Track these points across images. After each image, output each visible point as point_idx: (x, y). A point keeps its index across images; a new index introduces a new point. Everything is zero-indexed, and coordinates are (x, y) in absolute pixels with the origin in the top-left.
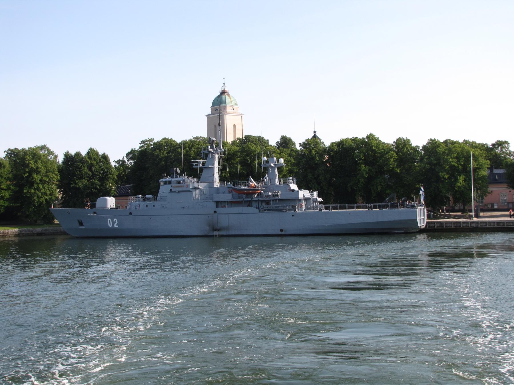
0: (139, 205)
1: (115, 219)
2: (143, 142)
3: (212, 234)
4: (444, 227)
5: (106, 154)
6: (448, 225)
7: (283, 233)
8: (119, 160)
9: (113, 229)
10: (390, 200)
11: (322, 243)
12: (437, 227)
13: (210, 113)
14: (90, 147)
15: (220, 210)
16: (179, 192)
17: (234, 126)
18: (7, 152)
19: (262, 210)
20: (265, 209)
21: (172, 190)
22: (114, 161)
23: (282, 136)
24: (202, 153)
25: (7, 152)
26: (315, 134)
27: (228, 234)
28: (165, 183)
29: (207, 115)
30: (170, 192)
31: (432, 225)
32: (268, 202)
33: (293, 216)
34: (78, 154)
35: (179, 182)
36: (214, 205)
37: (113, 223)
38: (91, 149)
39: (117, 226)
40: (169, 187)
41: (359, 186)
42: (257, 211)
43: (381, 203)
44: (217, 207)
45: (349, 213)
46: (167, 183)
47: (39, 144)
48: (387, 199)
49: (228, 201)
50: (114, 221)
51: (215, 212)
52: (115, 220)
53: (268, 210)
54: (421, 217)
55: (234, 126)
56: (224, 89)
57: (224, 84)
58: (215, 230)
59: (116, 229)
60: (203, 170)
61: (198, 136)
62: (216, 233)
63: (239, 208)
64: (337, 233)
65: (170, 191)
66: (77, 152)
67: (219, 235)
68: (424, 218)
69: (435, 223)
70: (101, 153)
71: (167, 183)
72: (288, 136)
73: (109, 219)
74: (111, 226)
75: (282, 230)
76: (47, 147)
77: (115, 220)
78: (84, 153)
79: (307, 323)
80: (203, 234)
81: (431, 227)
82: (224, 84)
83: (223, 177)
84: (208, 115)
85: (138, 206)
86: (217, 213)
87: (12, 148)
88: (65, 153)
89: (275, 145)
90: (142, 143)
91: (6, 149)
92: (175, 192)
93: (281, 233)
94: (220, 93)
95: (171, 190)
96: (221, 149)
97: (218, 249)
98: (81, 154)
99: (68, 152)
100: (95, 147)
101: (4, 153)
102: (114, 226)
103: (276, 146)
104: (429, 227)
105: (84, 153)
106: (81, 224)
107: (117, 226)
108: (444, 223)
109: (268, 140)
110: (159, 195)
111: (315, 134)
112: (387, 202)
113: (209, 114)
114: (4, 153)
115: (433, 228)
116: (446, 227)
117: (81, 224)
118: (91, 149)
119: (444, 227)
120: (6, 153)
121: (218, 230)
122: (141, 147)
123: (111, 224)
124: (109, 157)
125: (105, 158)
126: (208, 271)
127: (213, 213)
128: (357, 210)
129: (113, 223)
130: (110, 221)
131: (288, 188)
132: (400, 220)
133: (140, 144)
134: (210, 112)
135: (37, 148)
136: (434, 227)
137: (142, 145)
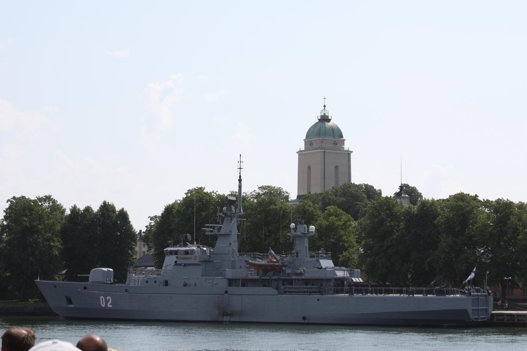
0: (138, 280)
1: (108, 297)
3: (222, 320)
4: (516, 320)
5: (125, 210)
6: (521, 318)
7: (306, 321)
8: (156, 217)
9: (106, 309)
10: (436, 285)
11: (248, 328)
12: (508, 320)
13: (303, 149)
14: (104, 201)
15: (233, 290)
16: (185, 265)
17: (337, 167)
18: (11, 201)
19: (282, 292)
20: (286, 290)
21: (178, 262)
22: (149, 217)
24: (218, 215)
25: (11, 201)
27: (240, 320)
28: (171, 253)
29: (299, 152)
30: (174, 265)
31: (501, 318)
32: (290, 282)
33: (318, 300)
35: (186, 252)
36: (225, 283)
37: (107, 302)
38: (105, 203)
39: (111, 306)
40: (173, 258)
41: (439, 263)
42: (276, 292)
43: (425, 287)
44: (230, 285)
45: (386, 299)
46: (173, 253)
47: (42, 195)
48: (432, 283)
49: (242, 278)
50: (108, 299)
51: (226, 292)
52: (109, 299)
53: (289, 292)
54: (478, 307)
55: (337, 167)
56: (325, 114)
57: (325, 106)
58: (226, 315)
59: (110, 309)
60: (218, 237)
61: (264, 185)
62: (227, 319)
63: (255, 288)
64: (279, 321)
65: (174, 264)
66: (86, 207)
67: (229, 322)
68: (487, 308)
69: (505, 315)
70: (118, 208)
71: (169, 254)
73: (102, 297)
74: (103, 306)
75: (304, 318)
76: (52, 199)
77: (109, 299)
78: (96, 208)
80: (211, 320)
81: (500, 320)
82: (325, 106)
83: (474, 226)
84: (300, 151)
85: (137, 282)
86: (229, 293)
87: (18, 196)
88: (71, 208)
91: (10, 197)
92: (180, 265)
93: (303, 321)
94: (319, 120)
95: (176, 262)
96: (241, 212)
97: (41, 325)
98: (92, 209)
100: (110, 201)
101: (7, 202)
102: (107, 305)
104: (497, 320)
105: (96, 208)
106: (70, 301)
107: (111, 306)
108: (516, 316)
109: (380, 190)
110: (163, 268)
112: (432, 287)
114: (7, 202)
115: (501, 322)
116: (518, 320)
117: (70, 301)
118: (105, 203)
119: (516, 320)
120: (9, 203)
121: (229, 315)
123: (104, 303)
124: (128, 214)
125: (123, 215)
127: (224, 293)
128: (395, 295)
129: (107, 302)
130: (102, 299)
131: (317, 265)
135: (40, 199)
136: (504, 320)
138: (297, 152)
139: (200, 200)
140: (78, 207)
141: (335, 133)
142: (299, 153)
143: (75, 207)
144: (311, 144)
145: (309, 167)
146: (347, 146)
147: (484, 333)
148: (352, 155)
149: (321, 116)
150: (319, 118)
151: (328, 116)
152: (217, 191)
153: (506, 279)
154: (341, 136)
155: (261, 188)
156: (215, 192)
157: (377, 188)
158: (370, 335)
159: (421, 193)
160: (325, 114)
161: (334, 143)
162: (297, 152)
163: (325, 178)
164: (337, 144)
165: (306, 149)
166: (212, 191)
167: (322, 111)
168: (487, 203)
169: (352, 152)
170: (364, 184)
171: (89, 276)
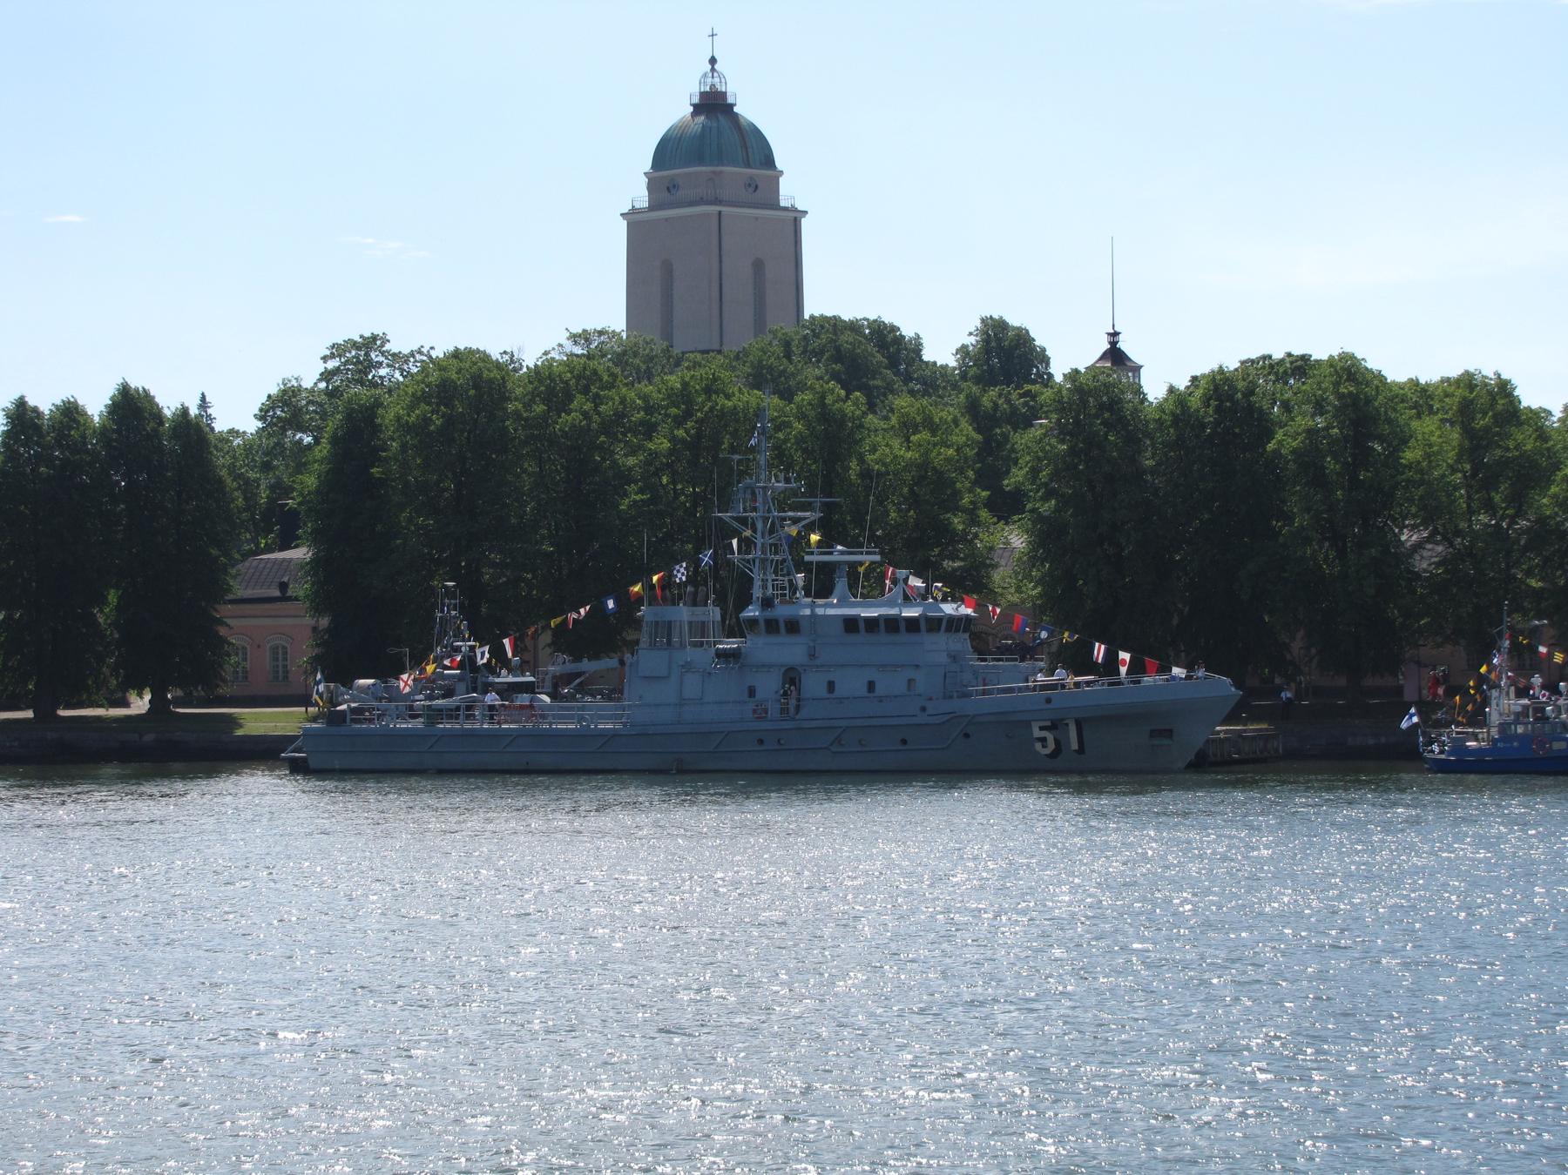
2: (337, 350)
17: (758, 266)
23: (983, 321)
26: (1113, 344)
34: (70, 412)
55: (758, 266)
56: (713, 86)
57: (713, 61)
72: (1014, 320)
79: (551, 724)
82: (713, 61)
89: (952, 362)
90: (332, 356)
99: (21, 404)
103: (955, 369)
105: (96, 405)
109: (918, 337)
111: (1113, 344)
113: (637, 206)
122: (327, 376)
126: (685, 1103)
132: (211, 773)
133: (325, 359)
134: (641, 197)
137: (332, 364)
138: (622, 215)
139: (477, 381)
140: (32, 401)
141: (750, 150)
142: (630, 216)
143: (21, 404)
144: (672, 187)
145: (668, 270)
146: (790, 191)
147: (1256, 782)
148: (805, 223)
149: (703, 95)
150: (696, 100)
151: (724, 95)
152: (432, 348)
153: (1537, 626)
154: (768, 161)
155: (574, 338)
156: (425, 352)
157: (907, 331)
158: (353, 802)
159: (1044, 350)
160: (713, 86)
161: (750, 185)
162: (622, 215)
163: (723, 300)
164: (757, 187)
165: (653, 207)
166: (415, 348)
167: (705, 75)
168: (1421, 397)
169: (806, 212)
170: (865, 319)
171: (858, 631)
